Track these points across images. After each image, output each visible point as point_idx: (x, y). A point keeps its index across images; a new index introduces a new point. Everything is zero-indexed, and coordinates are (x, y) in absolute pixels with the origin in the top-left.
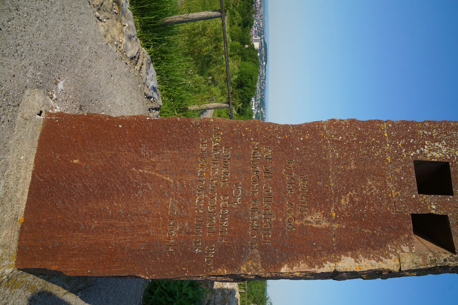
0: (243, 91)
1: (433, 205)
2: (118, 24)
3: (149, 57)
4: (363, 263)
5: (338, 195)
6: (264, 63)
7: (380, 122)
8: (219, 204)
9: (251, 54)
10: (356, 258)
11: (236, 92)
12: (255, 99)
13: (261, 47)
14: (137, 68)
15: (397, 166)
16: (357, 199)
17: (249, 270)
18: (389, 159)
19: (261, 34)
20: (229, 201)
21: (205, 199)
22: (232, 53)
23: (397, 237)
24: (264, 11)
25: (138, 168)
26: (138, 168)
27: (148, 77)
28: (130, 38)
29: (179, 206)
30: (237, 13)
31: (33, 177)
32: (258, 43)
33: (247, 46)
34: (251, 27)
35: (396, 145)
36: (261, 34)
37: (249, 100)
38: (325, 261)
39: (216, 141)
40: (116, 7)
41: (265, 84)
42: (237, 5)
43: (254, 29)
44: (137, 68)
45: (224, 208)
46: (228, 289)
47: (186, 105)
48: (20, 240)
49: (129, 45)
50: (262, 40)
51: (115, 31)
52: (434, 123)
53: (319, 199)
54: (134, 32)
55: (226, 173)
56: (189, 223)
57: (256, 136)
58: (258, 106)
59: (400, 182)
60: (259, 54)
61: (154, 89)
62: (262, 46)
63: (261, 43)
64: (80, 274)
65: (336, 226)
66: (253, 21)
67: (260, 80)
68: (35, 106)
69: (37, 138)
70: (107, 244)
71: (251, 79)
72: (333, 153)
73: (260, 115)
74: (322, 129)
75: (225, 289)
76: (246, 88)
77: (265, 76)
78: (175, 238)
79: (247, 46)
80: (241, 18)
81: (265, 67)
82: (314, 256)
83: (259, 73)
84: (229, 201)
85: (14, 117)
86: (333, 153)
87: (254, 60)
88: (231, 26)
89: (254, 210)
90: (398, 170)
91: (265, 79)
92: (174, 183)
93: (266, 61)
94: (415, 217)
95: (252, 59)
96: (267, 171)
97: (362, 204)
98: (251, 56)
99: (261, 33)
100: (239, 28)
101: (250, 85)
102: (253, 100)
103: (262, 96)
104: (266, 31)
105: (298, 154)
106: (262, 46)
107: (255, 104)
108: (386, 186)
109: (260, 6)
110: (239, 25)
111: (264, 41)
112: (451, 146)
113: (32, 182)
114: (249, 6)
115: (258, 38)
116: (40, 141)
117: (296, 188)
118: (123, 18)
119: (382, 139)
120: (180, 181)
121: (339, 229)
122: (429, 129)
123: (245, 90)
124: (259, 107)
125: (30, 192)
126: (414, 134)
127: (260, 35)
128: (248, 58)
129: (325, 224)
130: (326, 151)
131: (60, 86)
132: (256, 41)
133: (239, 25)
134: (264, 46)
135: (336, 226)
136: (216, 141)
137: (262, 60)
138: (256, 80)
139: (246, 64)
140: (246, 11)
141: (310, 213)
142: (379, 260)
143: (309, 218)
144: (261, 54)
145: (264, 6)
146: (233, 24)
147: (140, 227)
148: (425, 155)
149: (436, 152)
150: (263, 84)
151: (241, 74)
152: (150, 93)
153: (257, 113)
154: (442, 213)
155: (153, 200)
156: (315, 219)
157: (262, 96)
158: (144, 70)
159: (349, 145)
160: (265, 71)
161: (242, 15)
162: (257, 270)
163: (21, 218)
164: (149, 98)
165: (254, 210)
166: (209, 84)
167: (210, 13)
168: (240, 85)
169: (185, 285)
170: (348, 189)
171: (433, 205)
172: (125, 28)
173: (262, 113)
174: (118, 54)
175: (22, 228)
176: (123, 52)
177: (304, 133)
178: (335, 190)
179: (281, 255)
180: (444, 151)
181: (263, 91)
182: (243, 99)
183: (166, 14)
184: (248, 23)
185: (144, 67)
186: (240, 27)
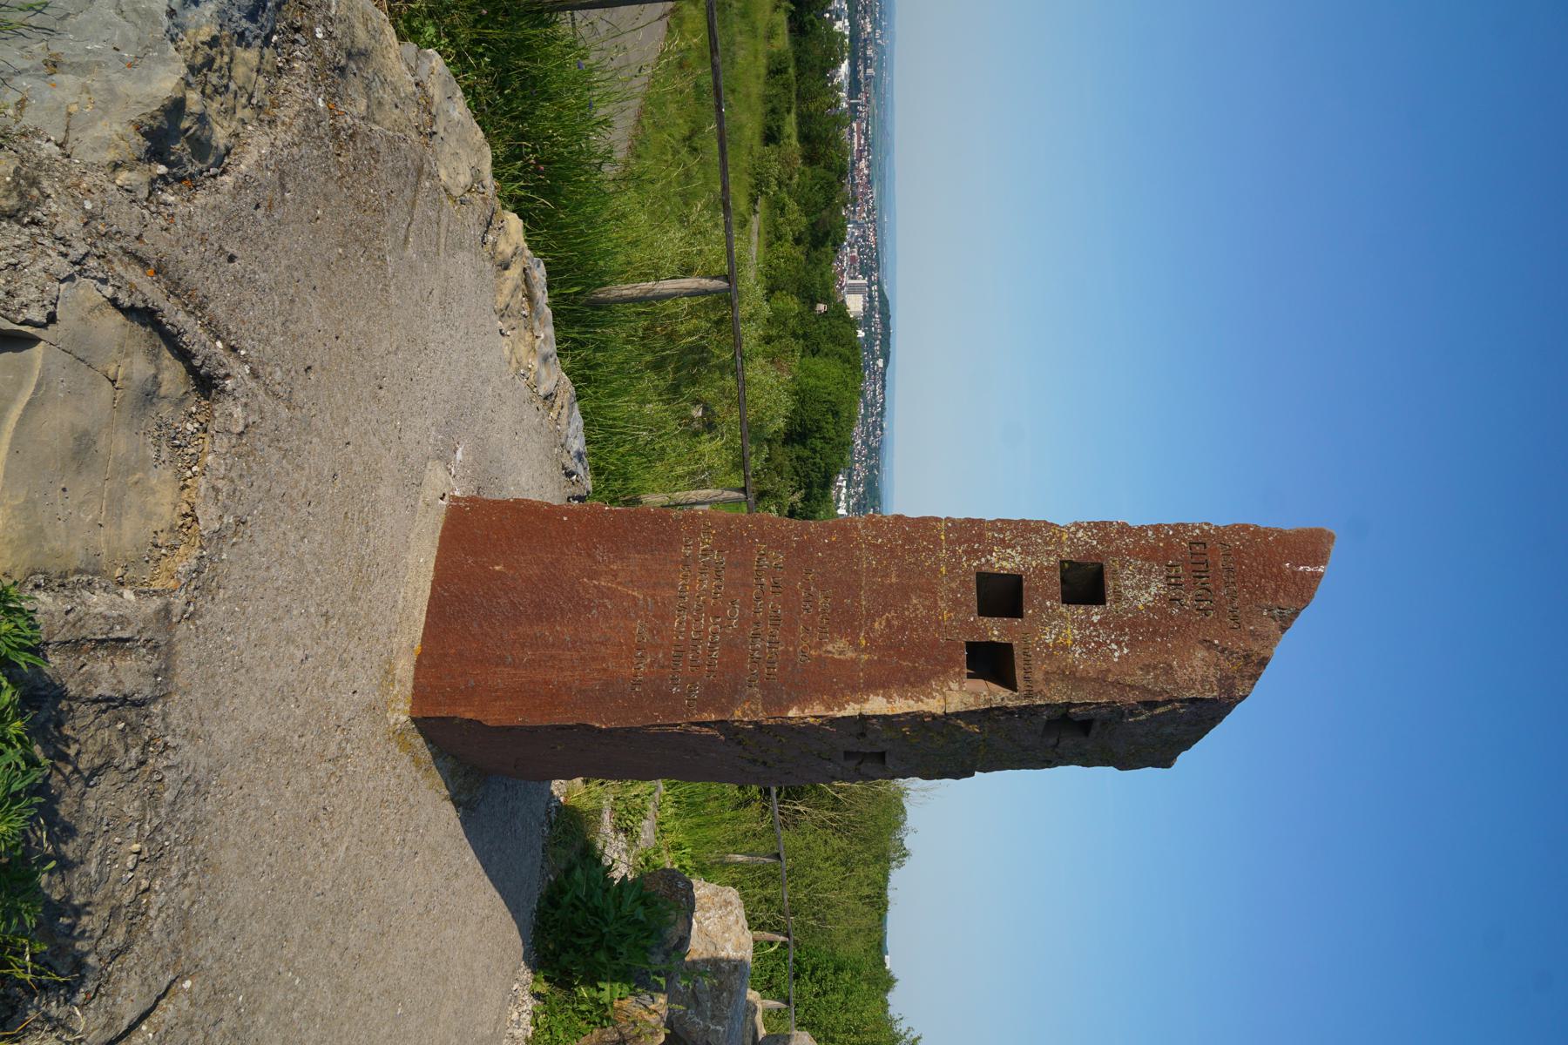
0: (807, 453)
1: (995, 630)
2: (528, 337)
3: (572, 389)
4: (898, 704)
5: (871, 617)
6: (880, 363)
7: (937, 520)
8: (706, 627)
9: (835, 332)
10: (889, 697)
11: (784, 456)
12: (849, 479)
14: (553, 415)
15: (953, 580)
16: (895, 623)
17: (745, 714)
18: (943, 569)
19: (872, 269)
20: (721, 624)
21: (688, 622)
22: (774, 332)
23: (945, 672)
24: (881, 195)
25: (591, 578)
26: (591, 578)
27: (570, 431)
28: (545, 359)
29: (651, 631)
30: (792, 205)
31: (433, 589)
32: (860, 297)
33: (821, 307)
34: (837, 245)
35: (954, 552)
36: (872, 269)
37: (827, 482)
38: (847, 702)
39: (706, 542)
40: (526, 305)
41: (882, 429)
42: (790, 178)
43: (848, 252)
44: (553, 415)
45: (714, 634)
46: (729, 961)
47: (641, 488)
48: (416, 678)
49: (544, 372)
50: (874, 288)
51: (522, 350)
52: (1009, 522)
53: (845, 622)
54: (552, 348)
55: (718, 587)
56: (665, 654)
57: (762, 536)
58: (857, 504)
59: (956, 602)
60: (861, 334)
61: (579, 456)
62: (872, 308)
63: (870, 296)
64: (507, 723)
65: (865, 657)
66: (844, 227)
67: (865, 417)
68: (444, 483)
69: (438, 534)
70: (546, 683)
71: (836, 414)
72: (869, 561)
74: (856, 528)
75: (722, 960)
76: (819, 444)
77: (883, 405)
78: (644, 674)
79: (821, 307)
80: (804, 219)
81: (884, 375)
82: (834, 696)
83: (862, 394)
84: (721, 624)
85: (416, 500)
86: (869, 561)
87: (846, 351)
88: (769, 245)
89: (755, 636)
90: (954, 585)
91: (881, 414)
92: (645, 600)
93: (886, 357)
94: (971, 647)
95: (840, 349)
96: (776, 585)
97: (902, 629)
98: (834, 339)
99: (870, 265)
100: (798, 252)
101: (832, 433)
102: (841, 481)
103: (871, 469)
104: (886, 259)
105: (821, 561)
106: (872, 308)
107: (849, 496)
108: (936, 605)
109: (869, 182)
110: (798, 241)
112: (1028, 554)
113: (432, 597)
114: (831, 185)
115: (862, 281)
116: (442, 538)
117: (815, 607)
118: (537, 324)
119: (937, 542)
120: (652, 596)
121: (869, 662)
122: (1001, 530)
123: (814, 451)
125: (428, 612)
126: (980, 537)
127: (866, 271)
128: (826, 347)
129: (850, 654)
130: (860, 559)
131: (459, 455)
132: (854, 290)
133: (798, 241)
134: (880, 307)
135: (865, 657)
136: (706, 542)
137: (873, 353)
139: (819, 364)
140: (820, 198)
141: (832, 640)
142: (920, 700)
143: (830, 648)
144: (869, 334)
145: (882, 179)
146: (779, 238)
147: (594, 659)
148: (992, 565)
149: (1006, 561)
150: (875, 429)
151: (802, 396)
152: (571, 466)
154: (1006, 640)
155: (613, 622)
156: (839, 648)
157: (871, 471)
158: (564, 419)
159: (891, 550)
160: (883, 387)
161: (808, 208)
162: (756, 714)
163: (417, 647)
164: (569, 474)
165: (755, 636)
166: (696, 434)
167: (704, 281)
168: (797, 434)
169: (629, 898)
170: (885, 609)
171: (995, 630)
172: (538, 342)
174: (527, 393)
175: (419, 661)
176: (533, 387)
177: (831, 534)
178: (868, 610)
179: (789, 694)
180: (1017, 559)
181: (875, 452)
182: (807, 476)
183: (601, 279)
184: (827, 234)
185: (565, 411)
186: (801, 248)
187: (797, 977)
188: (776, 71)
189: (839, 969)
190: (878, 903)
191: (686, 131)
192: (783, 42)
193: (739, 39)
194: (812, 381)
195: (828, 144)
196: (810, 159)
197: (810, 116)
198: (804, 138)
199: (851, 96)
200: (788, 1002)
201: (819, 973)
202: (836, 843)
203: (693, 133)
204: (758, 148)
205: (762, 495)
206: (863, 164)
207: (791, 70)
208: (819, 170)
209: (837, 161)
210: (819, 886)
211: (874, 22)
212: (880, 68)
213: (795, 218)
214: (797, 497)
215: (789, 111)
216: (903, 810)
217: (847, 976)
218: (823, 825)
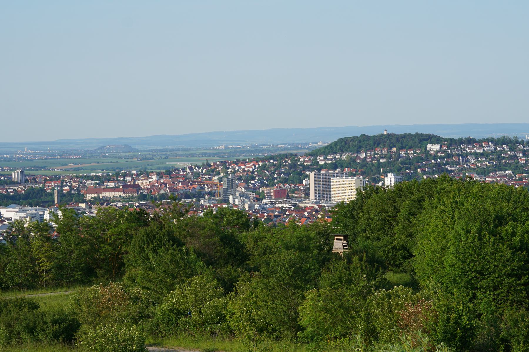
6: (433, 148)
13: (354, 168)
22: (361, 325)
24: (186, 156)
30: (172, 299)
33: (338, 245)
34: (243, 221)
67: (517, 168)
71: (500, 220)
77: (499, 142)
79: (338, 245)
81: (451, 142)
87: (405, 205)
88: (231, 333)
91: (513, 144)
98: (387, 224)
99: (286, 168)
104: (279, 144)
109: (169, 173)
111: (330, 149)
114: (151, 238)
132: (324, 192)
133: (229, 286)
134: (349, 151)
139: (424, 247)
145: (166, 154)
146: (222, 318)
160: (470, 142)
161: (180, 273)
194: (449, 259)
195: (101, 240)
196: (115, 268)
198: (88, 275)
199: (47, 203)
206: (143, 183)
208: (131, 252)
209: (123, 227)
213: (196, 290)
215: (33, 306)
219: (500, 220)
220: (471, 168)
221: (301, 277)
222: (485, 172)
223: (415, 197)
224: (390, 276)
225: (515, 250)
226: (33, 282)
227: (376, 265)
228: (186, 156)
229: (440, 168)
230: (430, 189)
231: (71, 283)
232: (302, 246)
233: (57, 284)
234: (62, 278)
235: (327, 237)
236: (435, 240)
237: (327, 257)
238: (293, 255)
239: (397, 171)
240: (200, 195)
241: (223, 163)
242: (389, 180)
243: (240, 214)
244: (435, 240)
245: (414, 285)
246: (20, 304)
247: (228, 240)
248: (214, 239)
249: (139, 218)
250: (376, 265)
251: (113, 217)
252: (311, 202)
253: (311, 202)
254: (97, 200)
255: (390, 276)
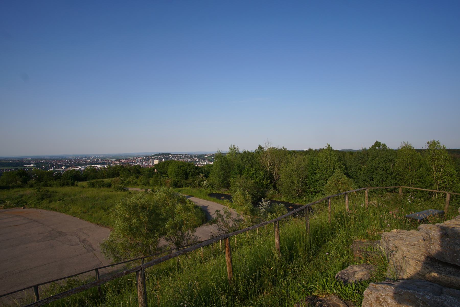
0: (191, 173)
6: (170, 155)
13: (158, 158)
22: (159, 183)
24: (130, 157)
30: (128, 180)
33: (156, 170)
34: (140, 167)
37: (197, 168)
62: (157, 158)
67: (183, 159)
71: (181, 167)
73: (210, 158)
76: (188, 171)
79: (156, 170)
81: (173, 155)
87: (166, 164)
88: (138, 185)
91: (183, 155)
98: (163, 167)
99: (147, 158)
103: (195, 157)
106: (157, 158)
107: (202, 162)
114: (124, 170)
123: (190, 171)
124: (204, 159)
132: (153, 162)
133: (138, 178)
134: (157, 156)
138: (182, 163)
139: (169, 171)
145: (127, 156)
146: (136, 183)
153: (209, 160)
161: (129, 176)
173: (209, 157)
181: (191, 156)
182: (197, 173)
187: (315, 174)
188: (93, 185)
189: (313, 164)
190: (294, 153)
191: (103, 211)
192: (85, 183)
193: (81, 196)
194: (173, 173)
195: (115, 170)
196: (118, 175)
197: (108, 175)
198: (113, 176)
199: (106, 164)
200: (346, 194)
201: (314, 169)
202: (282, 165)
203: (104, 209)
204: (111, 189)
205: (199, 185)
206: (123, 161)
207: (93, 181)
208: (121, 172)
209: (119, 168)
210: (293, 169)
211: (88, 159)
212: (99, 157)
213: (132, 178)
214: (202, 175)
215: (103, 182)
216: (273, 148)
217: (314, 162)
218: (279, 168)
219: (181, 167)
220: (176, 159)
221: (150, 176)
222: (178, 159)
223: (168, 163)
224: (164, 175)
225: (183, 171)
226: (103, 177)
227: (162, 173)
228: (130, 157)
229: (171, 159)
230: (170, 162)
231: (110, 177)
232: (150, 171)
233: (107, 178)
234: (108, 176)
235: (154, 170)
236: (171, 169)
237: (154, 173)
238: (148, 172)
239: (165, 159)
240: (132, 163)
241: (136, 158)
242: (163, 160)
243: (139, 166)
244: (171, 169)
245: (168, 176)
246: (101, 181)
247: (137, 170)
248: (163, 254)
249: (122, 167)
250: (162, 173)
251: (118, 166)
252: (151, 164)
253: (151, 164)
254: (114, 164)
255: (164, 175)
